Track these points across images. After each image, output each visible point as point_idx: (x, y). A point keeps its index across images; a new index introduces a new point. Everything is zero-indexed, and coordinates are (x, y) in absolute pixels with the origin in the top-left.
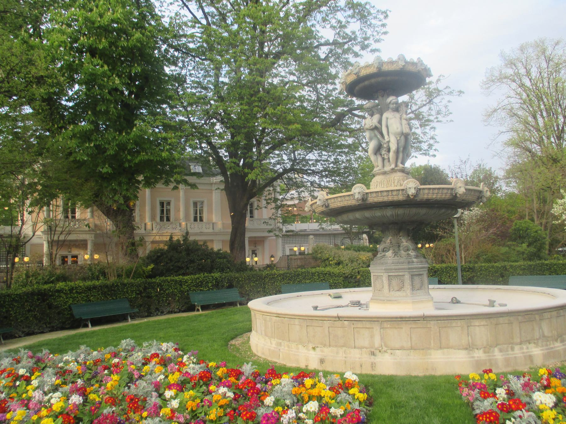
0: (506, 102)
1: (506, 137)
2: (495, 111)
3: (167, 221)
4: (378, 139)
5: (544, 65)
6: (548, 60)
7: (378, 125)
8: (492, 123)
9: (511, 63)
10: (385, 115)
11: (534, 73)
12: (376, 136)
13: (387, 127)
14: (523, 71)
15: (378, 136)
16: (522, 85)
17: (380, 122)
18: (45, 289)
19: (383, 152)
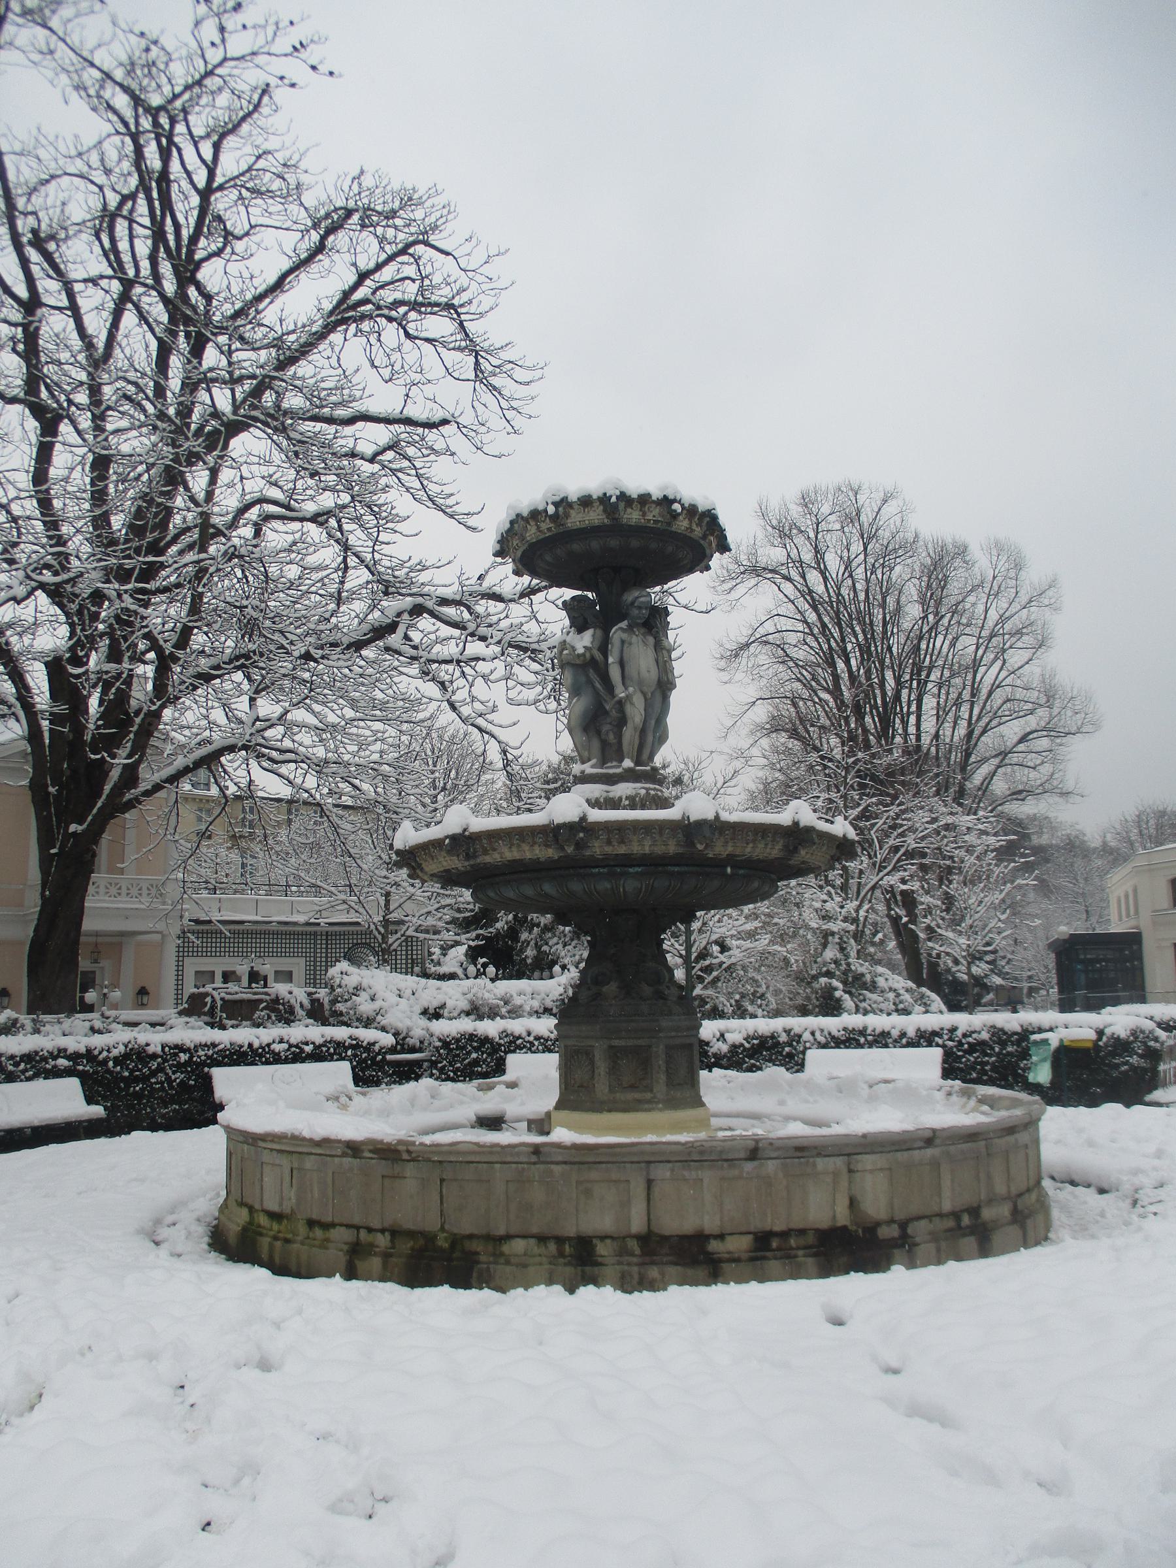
0: (769, 627)
1: (761, 713)
2: (748, 645)
3: (1133, 988)
4: (596, 692)
5: (856, 547)
6: (867, 538)
7: (598, 656)
8: (739, 676)
9: (784, 532)
10: (617, 633)
11: (833, 563)
12: (590, 682)
13: (622, 664)
14: (808, 556)
15: (598, 685)
16: (808, 593)
17: (604, 648)
18: (422, 1144)
19: (605, 728)
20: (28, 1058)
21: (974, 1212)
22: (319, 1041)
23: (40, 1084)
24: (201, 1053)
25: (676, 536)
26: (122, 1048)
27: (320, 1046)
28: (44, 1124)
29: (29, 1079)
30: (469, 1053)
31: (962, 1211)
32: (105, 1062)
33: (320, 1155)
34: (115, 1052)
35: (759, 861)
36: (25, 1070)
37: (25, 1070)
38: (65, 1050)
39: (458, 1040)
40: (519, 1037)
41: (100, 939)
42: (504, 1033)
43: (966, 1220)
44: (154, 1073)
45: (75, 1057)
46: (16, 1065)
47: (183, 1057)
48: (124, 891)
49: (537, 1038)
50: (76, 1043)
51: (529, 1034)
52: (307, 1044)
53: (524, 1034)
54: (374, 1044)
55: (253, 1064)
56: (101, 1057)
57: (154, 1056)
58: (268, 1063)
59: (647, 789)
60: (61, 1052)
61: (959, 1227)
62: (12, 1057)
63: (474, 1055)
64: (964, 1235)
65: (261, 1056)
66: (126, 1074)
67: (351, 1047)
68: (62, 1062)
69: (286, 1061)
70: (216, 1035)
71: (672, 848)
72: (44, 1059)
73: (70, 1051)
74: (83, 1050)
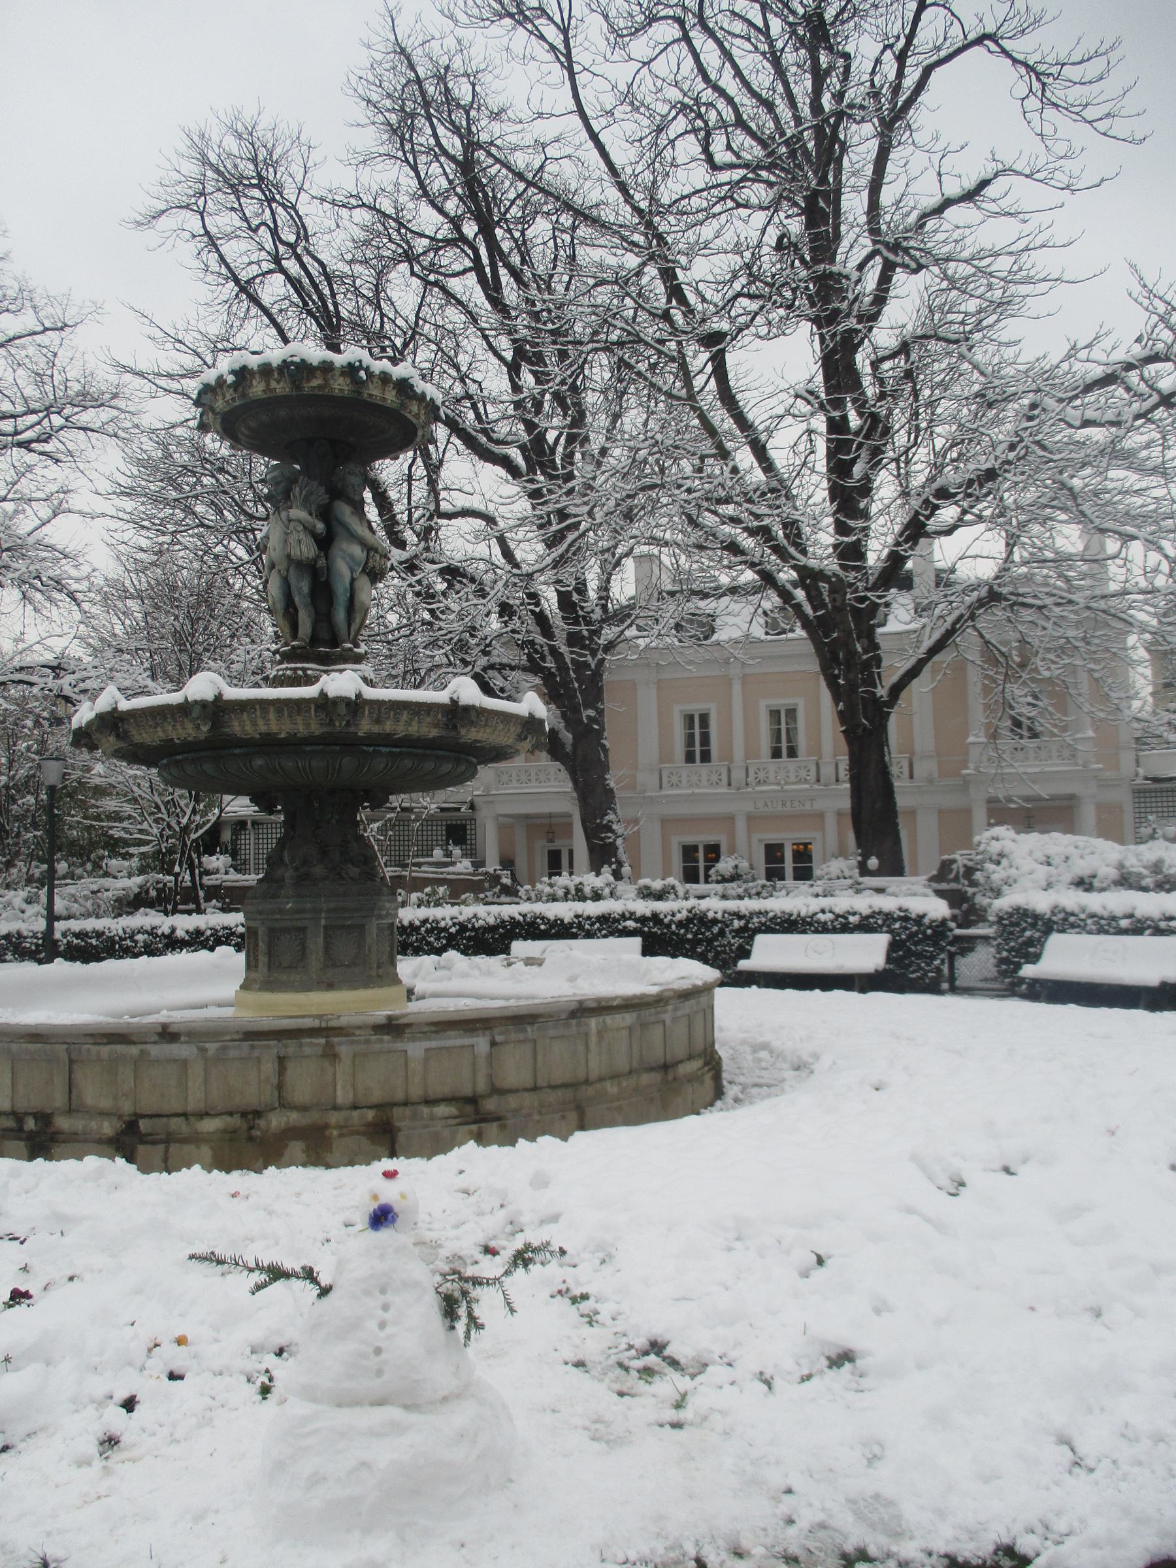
20: (604, 919)
21: (44, 1118)
22: (866, 911)
23: (612, 941)
24: (755, 920)
25: (259, 404)
26: (685, 914)
27: (867, 917)
28: (1084, 980)
29: (605, 936)
30: (1024, 930)
31: (26, 1114)
32: (668, 926)
33: (303, 1017)
34: (679, 917)
35: (419, 739)
36: (600, 930)
37: (600, 930)
38: (632, 914)
39: (1011, 915)
40: (1073, 914)
41: (554, 821)
42: (1055, 910)
43: (30, 1124)
44: (715, 937)
45: (643, 920)
46: (592, 924)
47: (737, 924)
48: (533, 777)
49: (1092, 916)
50: (888, 904)
51: (1083, 911)
52: (854, 914)
53: (1076, 911)
54: (924, 916)
55: (804, 932)
56: (666, 921)
57: (715, 921)
58: (816, 931)
59: (295, 669)
60: (632, 916)
61: (21, 1129)
62: (589, 918)
63: (1028, 934)
64: (19, 1139)
65: (810, 924)
66: (690, 936)
67: (901, 919)
68: (631, 924)
69: (834, 931)
70: (748, 905)
71: (316, 729)
72: (618, 921)
73: (638, 914)
74: (648, 914)
